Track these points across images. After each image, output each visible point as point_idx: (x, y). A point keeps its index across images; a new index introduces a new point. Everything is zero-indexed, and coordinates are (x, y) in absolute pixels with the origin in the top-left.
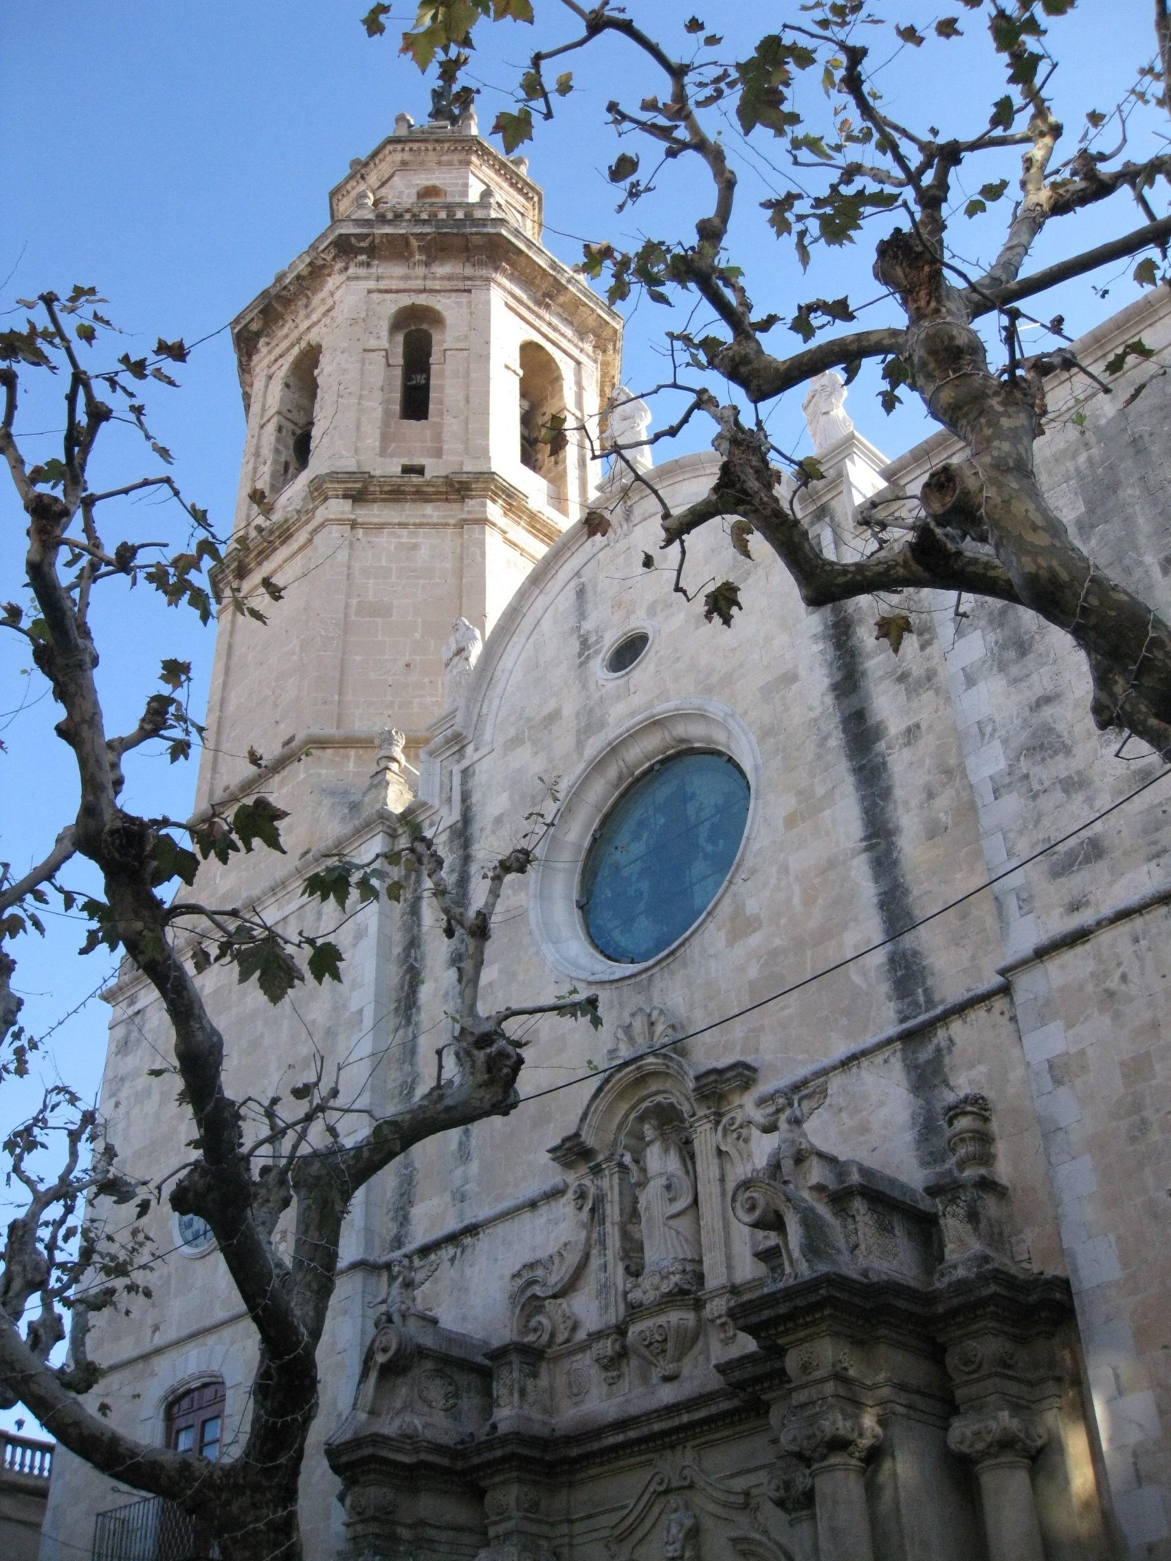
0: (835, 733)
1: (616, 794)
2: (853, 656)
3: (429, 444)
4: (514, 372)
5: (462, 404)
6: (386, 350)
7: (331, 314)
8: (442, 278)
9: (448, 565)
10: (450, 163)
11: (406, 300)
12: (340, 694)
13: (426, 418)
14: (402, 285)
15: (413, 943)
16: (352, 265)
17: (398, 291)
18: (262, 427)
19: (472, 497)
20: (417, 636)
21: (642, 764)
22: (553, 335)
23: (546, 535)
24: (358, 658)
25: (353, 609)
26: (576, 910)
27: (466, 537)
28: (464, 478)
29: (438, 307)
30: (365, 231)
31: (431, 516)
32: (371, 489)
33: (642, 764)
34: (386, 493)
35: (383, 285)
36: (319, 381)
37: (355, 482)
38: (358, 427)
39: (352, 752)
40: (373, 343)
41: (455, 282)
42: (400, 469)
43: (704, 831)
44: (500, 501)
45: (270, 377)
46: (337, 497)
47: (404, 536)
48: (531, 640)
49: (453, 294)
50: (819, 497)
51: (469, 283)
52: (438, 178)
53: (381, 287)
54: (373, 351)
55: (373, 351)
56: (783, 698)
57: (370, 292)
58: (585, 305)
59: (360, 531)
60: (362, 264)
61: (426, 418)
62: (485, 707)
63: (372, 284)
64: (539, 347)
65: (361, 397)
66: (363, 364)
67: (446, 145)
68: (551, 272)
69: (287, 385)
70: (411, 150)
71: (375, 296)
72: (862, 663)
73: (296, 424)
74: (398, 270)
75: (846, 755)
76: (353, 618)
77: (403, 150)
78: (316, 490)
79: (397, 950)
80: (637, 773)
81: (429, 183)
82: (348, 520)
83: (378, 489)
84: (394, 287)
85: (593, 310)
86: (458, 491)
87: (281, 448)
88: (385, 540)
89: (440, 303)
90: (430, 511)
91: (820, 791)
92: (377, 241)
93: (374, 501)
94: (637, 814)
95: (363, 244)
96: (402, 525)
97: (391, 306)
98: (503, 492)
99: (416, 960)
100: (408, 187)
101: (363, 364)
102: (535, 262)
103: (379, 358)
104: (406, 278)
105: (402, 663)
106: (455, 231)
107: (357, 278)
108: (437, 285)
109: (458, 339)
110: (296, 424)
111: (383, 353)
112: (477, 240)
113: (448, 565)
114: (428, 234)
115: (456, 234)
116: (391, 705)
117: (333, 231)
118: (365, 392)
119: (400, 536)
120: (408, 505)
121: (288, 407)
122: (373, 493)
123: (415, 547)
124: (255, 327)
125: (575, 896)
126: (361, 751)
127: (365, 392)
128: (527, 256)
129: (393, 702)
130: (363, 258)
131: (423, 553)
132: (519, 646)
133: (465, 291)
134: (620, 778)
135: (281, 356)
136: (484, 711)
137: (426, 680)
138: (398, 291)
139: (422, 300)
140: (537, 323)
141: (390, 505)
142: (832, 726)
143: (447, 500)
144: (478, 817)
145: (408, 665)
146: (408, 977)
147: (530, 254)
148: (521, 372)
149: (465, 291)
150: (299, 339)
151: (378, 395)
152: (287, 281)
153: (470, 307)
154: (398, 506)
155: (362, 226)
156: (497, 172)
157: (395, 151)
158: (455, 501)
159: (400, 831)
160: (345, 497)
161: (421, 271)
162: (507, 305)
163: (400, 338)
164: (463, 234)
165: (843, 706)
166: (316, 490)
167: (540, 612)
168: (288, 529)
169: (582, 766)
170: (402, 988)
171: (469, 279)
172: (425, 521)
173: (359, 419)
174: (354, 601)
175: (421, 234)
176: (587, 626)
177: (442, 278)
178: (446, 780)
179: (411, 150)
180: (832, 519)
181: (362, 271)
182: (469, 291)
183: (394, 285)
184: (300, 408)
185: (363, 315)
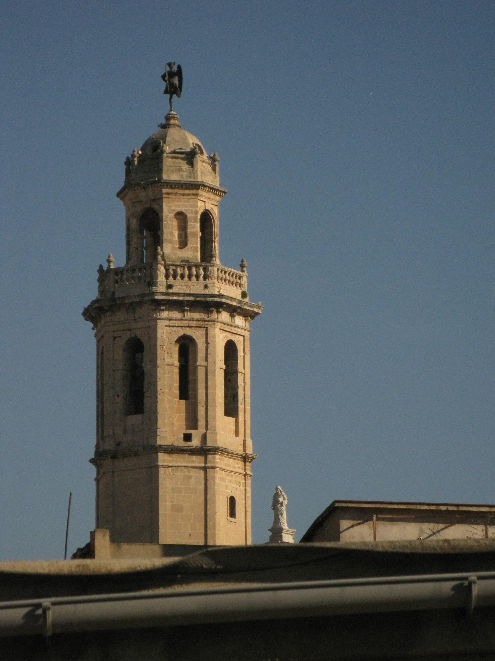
11: (181, 332)
29: (194, 337)
35: (172, 323)
42: (182, 436)
51: (206, 323)
53: (171, 325)
88: (179, 473)
96: (185, 467)
105: (187, 534)
108: (194, 324)
123: (190, 477)
131: (193, 480)
141: (180, 455)
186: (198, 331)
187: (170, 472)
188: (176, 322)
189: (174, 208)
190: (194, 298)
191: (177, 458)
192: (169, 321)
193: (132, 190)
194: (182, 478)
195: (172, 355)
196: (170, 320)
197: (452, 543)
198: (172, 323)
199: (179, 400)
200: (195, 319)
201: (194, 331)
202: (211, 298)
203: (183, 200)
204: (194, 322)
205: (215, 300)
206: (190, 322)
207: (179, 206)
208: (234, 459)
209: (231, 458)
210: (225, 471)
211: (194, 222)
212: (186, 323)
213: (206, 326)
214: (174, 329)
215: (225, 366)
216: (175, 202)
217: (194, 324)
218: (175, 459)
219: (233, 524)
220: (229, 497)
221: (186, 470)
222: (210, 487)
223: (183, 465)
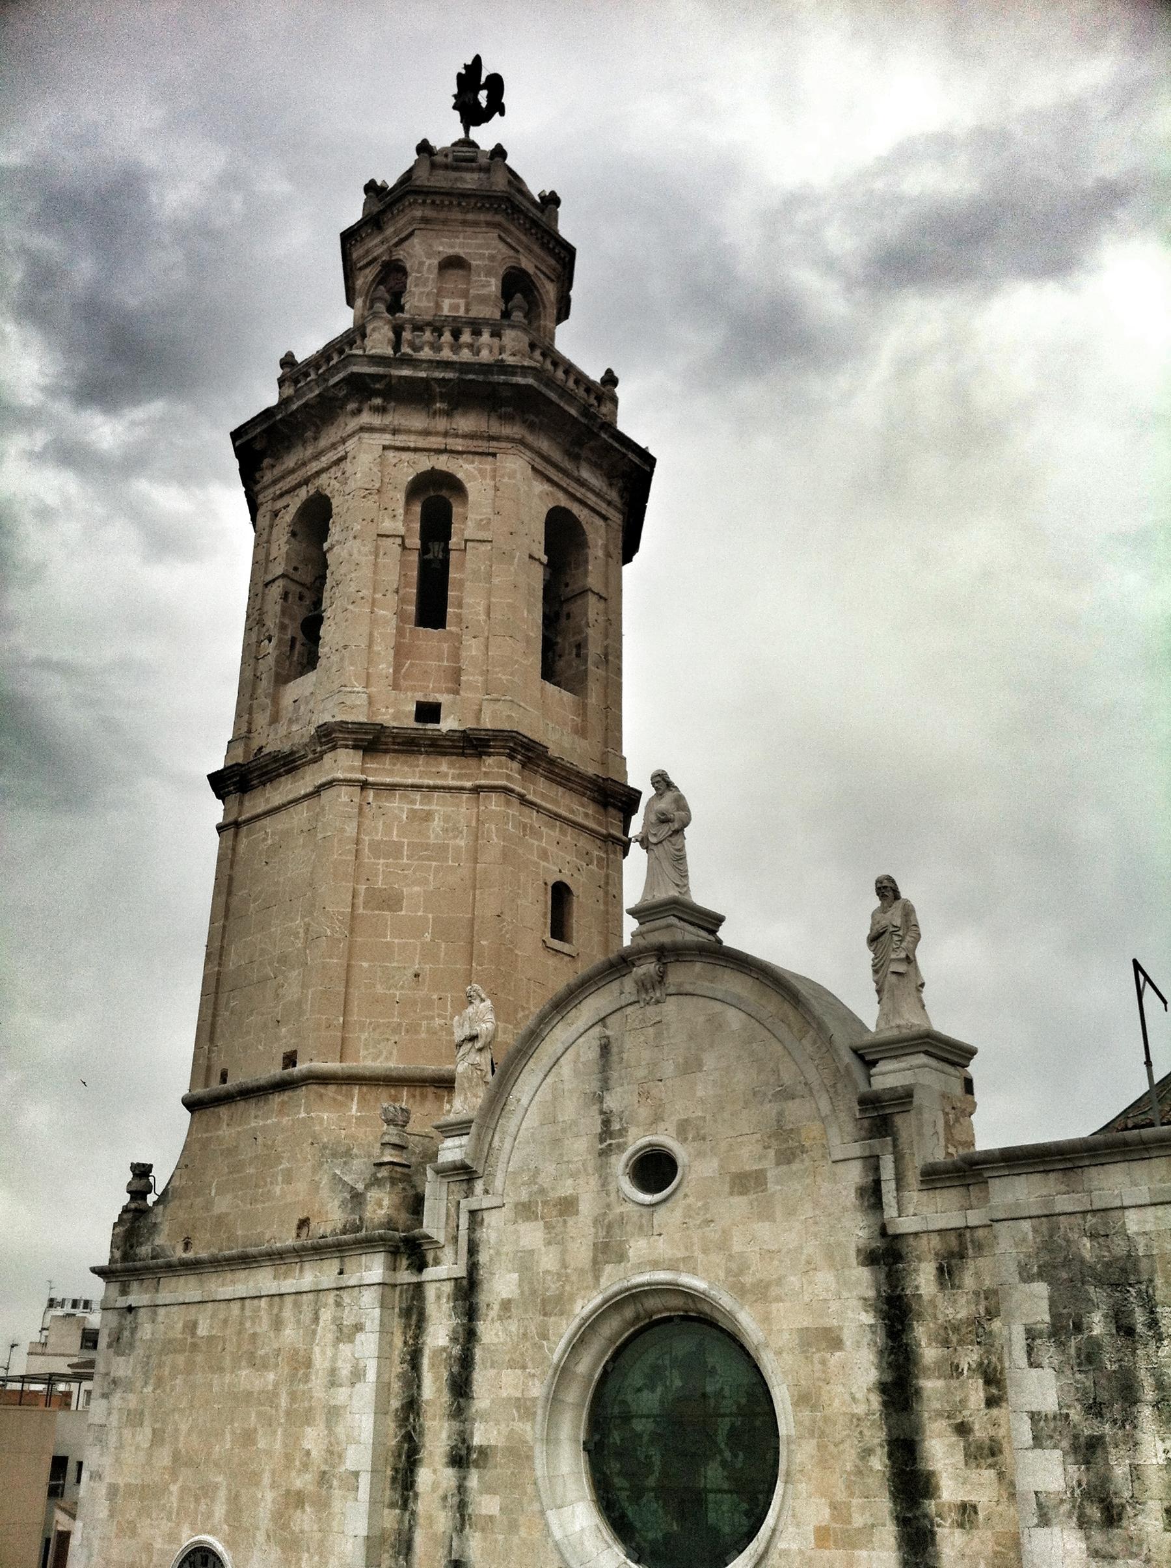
0: (879, 1451)
1: (632, 1330)
2: (907, 1359)
3: (445, 663)
4: (539, 560)
5: (482, 617)
6: (402, 537)
7: (342, 465)
8: (465, 436)
9: (462, 843)
10: (476, 224)
11: (425, 463)
12: (344, 1015)
13: (444, 627)
14: (421, 442)
15: (412, 1406)
16: (366, 407)
17: (416, 450)
18: (266, 585)
19: (490, 754)
20: (428, 937)
21: (660, 1312)
22: (580, 492)
23: (563, 777)
24: (365, 965)
25: (360, 900)
26: (582, 1454)
27: (482, 808)
28: (482, 735)
29: (460, 475)
30: (380, 370)
31: (446, 775)
32: (383, 739)
33: (660, 1312)
34: (399, 744)
35: (400, 440)
36: (330, 558)
37: (366, 733)
38: (370, 646)
39: (356, 1090)
40: (388, 525)
41: (480, 443)
42: (413, 708)
43: (724, 1425)
44: (519, 757)
45: (276, 514)
46: (347, 747)
47: (418, 802)
48: (549, 1080)
49: (477, 458)
50: (883, 1107)
51: (495, 444)
52: (462, 245)
53: (398, 444)
54: (388, 536)
55: (388, 536)
56: (824, 1362)
57: (385, 448)
58: (616, 449)
59: (371, 793)
60: (377, 410)
61: (444, 627)
62: (496, 1138)
63: (387, 439)
64: (566, 512)
65: (374, 603)
66: (377, 556)
67: (473, 201)
68: (583, 420)
69: (294, 534)
70: (433, 202)
71: (391, 454)
72: (917, 1378)
73: (303, 585)
74: (418, 421)
75: (891, 1492)
76: (361, 911)
77: (424, 202)
78: (325, 736)
79: (395, 1404)
80: (655, 1317)
81: (451, 251)
82: (359, 781)
83: (390, 739)
84: (412, 445)
85: (625, 455)
86: (475, 747)
87: (287, 621)
88: (397, 805)
89: (464, 469)
90: (447, 771)
91: (858, 1521)
92: (393, 382)
93: (386, 751)
94: (650, 1358)
95: (378, 386)
96: (416, 787)
97: (408, 468)
98: (522, 747)
99: (414, 1428)
100: (429, 256)
101: (377, 556)
102: (566, 411)
103: (393, 545)
104: (426, 433)
105: (410, 973)
106: (481, 378)
107: (371, 429)
108: (458, 444)
109: (480, 525)
110: (303, 585)
111: (399, 541)
112: (507, 393)
113: (462, 843)
114: (450, 380)
115: (484, 382)
116: (396, 1029)
117: (345, 367)
118: (378, 596)
119: (413, 802)
120: (422, 760)
121: (295, 564)
122: (386, 743)
123: (428, 816)
124: (258, 446)
125: (582, 1437)
126: (365, 1089)
127: (378, 596)
128: (558, 406)
129: (400, 1024)
130: (378, 401)
131: (437, 824)
132: (535, 1081)
133: (489, 454)
134: (637, 1318)
135: (288, 492)
136: (496, 1143)
137: (435, 997)
138: (416, 450)
139: (442, 463)
140: (564, 482)
141: (402, 758)
142: (877, 1441)
143: (463, 755)
144: (485, 1286)
145: (417, 975)
146: (406, 1446)
147: (562, 404)
148: (545, 559)
149: (489, 454)
150: (306, 482)
151: (393, 599)
152: (294, 407)
153: (494, 478)
154: (411, 759)
155: (378, 364)
156: (526, 232)
157: (415, 202)
158: (471, 755)
159: (402, 1249)
160: (355, 747)
161: (441, 424)
162: (533, 468)
163: (417, 509)
164: (490, 383)
165: (891, 1422)
166: (325, 736)
167: (560, 1048)
168: (294, 761)
169: (598, 1299)
170: (400, 1456)
171: (492, 438)
172: (440, 782)
173: (371, 635)
174: (362, 888)
175: (443, 379)
176: (612, 1102)
177: (465, 436)
178: (453, 1210)
179: (433, 202)
180: (895, 1140)
181: (377, 420)
182: (494, 455)
183: (412, 441)
184: (306, 561)
185: (377, 485)
186: (473, 462)
187: (370, 800)
188: (413, 438)
189: (441, 249)
190: (457, 375)
191: (394, 765)
192: (394, 434)
193: (356, 240)
194: (404, 817)
195: (395, 513)
196: (395, 432)
197: (727, 1529)
198: (400, 440)
199: (416, 626)
200: (460, 432)
201: (460, 461)
202: (502, 377)
203: (461, 235)
204: (459, 441)
205: (514, 382)
206: (450, 441)
207: (452, 247)
208: (571, 789)
209: (559, 784)
210: (538, 812)
211: (486, 276)
212: (436, 442)
213: (491, 450)
214: (405, 456)
215: (546, 557)
216: (443, 237)
217: (458, 444)
218: (387, 767)
219: (562, 959)
220: (551, 883)
221: (418, 796)
222: (485, 841)
223: (410, 781)
